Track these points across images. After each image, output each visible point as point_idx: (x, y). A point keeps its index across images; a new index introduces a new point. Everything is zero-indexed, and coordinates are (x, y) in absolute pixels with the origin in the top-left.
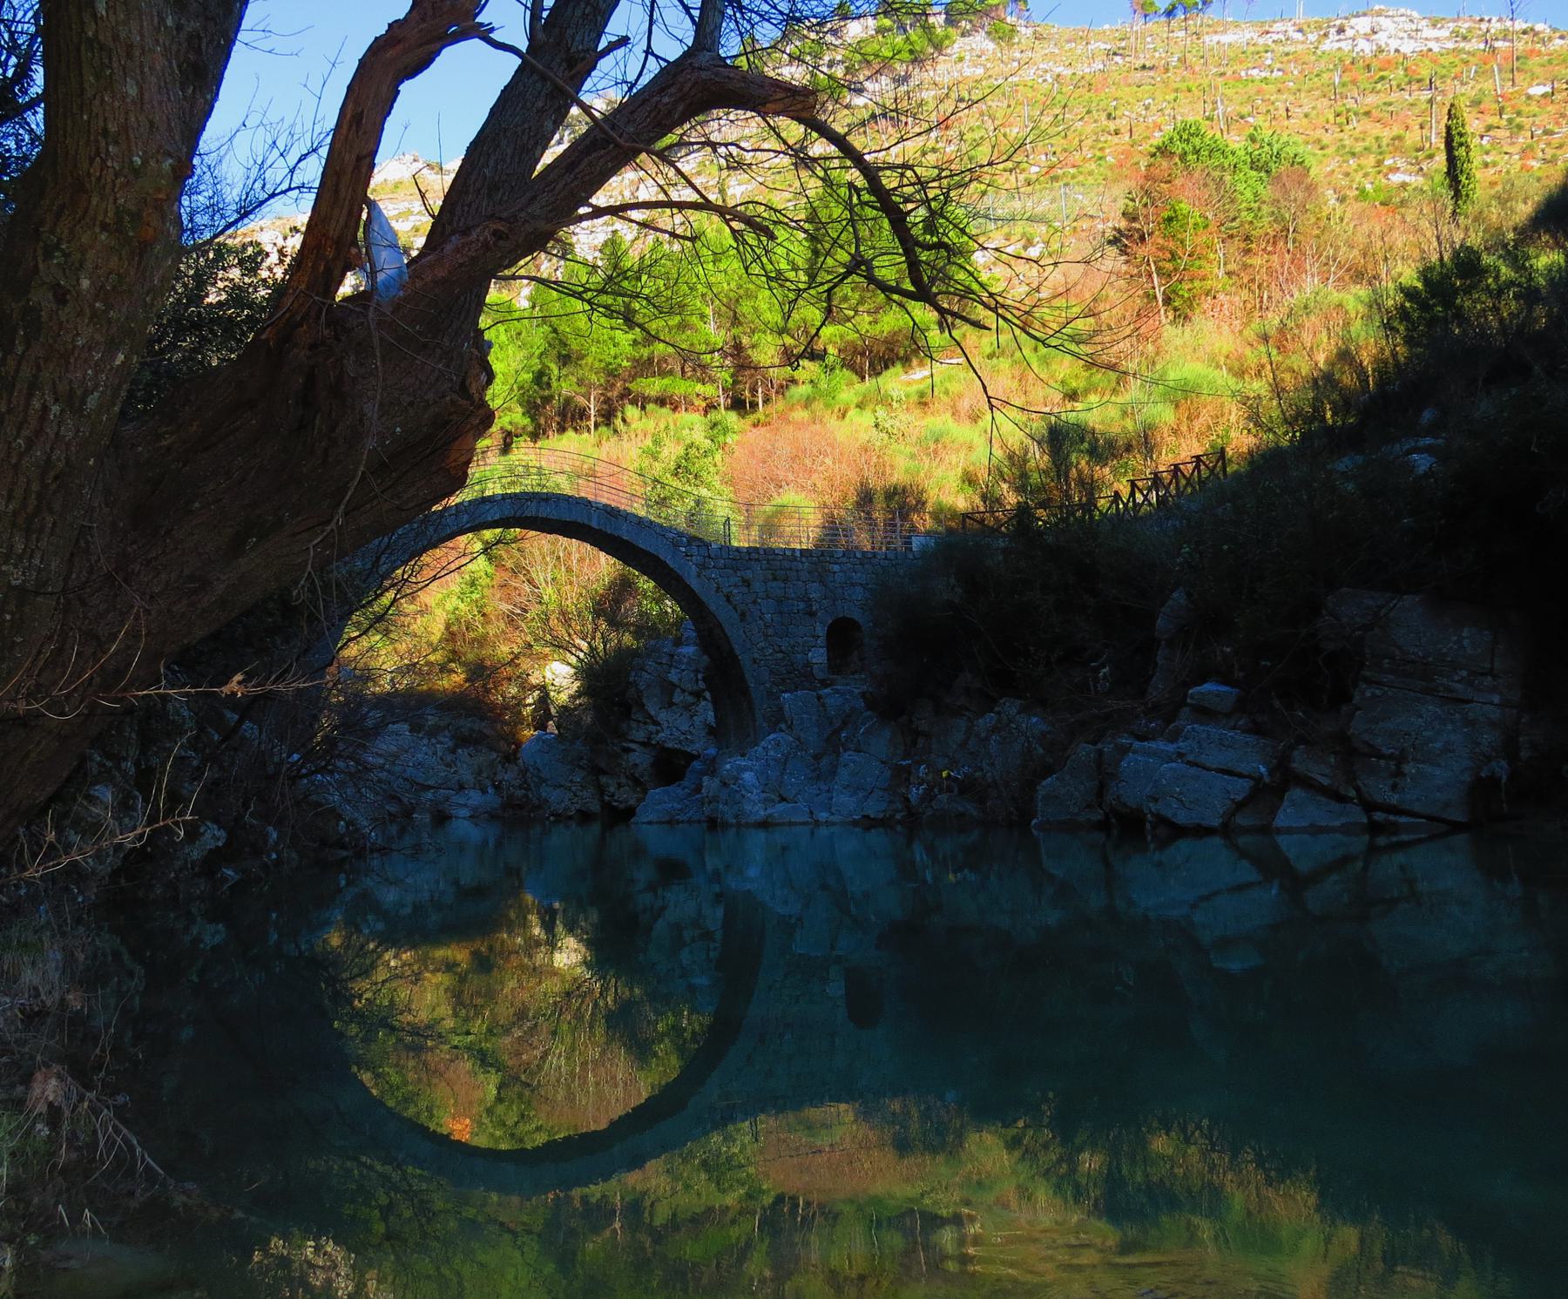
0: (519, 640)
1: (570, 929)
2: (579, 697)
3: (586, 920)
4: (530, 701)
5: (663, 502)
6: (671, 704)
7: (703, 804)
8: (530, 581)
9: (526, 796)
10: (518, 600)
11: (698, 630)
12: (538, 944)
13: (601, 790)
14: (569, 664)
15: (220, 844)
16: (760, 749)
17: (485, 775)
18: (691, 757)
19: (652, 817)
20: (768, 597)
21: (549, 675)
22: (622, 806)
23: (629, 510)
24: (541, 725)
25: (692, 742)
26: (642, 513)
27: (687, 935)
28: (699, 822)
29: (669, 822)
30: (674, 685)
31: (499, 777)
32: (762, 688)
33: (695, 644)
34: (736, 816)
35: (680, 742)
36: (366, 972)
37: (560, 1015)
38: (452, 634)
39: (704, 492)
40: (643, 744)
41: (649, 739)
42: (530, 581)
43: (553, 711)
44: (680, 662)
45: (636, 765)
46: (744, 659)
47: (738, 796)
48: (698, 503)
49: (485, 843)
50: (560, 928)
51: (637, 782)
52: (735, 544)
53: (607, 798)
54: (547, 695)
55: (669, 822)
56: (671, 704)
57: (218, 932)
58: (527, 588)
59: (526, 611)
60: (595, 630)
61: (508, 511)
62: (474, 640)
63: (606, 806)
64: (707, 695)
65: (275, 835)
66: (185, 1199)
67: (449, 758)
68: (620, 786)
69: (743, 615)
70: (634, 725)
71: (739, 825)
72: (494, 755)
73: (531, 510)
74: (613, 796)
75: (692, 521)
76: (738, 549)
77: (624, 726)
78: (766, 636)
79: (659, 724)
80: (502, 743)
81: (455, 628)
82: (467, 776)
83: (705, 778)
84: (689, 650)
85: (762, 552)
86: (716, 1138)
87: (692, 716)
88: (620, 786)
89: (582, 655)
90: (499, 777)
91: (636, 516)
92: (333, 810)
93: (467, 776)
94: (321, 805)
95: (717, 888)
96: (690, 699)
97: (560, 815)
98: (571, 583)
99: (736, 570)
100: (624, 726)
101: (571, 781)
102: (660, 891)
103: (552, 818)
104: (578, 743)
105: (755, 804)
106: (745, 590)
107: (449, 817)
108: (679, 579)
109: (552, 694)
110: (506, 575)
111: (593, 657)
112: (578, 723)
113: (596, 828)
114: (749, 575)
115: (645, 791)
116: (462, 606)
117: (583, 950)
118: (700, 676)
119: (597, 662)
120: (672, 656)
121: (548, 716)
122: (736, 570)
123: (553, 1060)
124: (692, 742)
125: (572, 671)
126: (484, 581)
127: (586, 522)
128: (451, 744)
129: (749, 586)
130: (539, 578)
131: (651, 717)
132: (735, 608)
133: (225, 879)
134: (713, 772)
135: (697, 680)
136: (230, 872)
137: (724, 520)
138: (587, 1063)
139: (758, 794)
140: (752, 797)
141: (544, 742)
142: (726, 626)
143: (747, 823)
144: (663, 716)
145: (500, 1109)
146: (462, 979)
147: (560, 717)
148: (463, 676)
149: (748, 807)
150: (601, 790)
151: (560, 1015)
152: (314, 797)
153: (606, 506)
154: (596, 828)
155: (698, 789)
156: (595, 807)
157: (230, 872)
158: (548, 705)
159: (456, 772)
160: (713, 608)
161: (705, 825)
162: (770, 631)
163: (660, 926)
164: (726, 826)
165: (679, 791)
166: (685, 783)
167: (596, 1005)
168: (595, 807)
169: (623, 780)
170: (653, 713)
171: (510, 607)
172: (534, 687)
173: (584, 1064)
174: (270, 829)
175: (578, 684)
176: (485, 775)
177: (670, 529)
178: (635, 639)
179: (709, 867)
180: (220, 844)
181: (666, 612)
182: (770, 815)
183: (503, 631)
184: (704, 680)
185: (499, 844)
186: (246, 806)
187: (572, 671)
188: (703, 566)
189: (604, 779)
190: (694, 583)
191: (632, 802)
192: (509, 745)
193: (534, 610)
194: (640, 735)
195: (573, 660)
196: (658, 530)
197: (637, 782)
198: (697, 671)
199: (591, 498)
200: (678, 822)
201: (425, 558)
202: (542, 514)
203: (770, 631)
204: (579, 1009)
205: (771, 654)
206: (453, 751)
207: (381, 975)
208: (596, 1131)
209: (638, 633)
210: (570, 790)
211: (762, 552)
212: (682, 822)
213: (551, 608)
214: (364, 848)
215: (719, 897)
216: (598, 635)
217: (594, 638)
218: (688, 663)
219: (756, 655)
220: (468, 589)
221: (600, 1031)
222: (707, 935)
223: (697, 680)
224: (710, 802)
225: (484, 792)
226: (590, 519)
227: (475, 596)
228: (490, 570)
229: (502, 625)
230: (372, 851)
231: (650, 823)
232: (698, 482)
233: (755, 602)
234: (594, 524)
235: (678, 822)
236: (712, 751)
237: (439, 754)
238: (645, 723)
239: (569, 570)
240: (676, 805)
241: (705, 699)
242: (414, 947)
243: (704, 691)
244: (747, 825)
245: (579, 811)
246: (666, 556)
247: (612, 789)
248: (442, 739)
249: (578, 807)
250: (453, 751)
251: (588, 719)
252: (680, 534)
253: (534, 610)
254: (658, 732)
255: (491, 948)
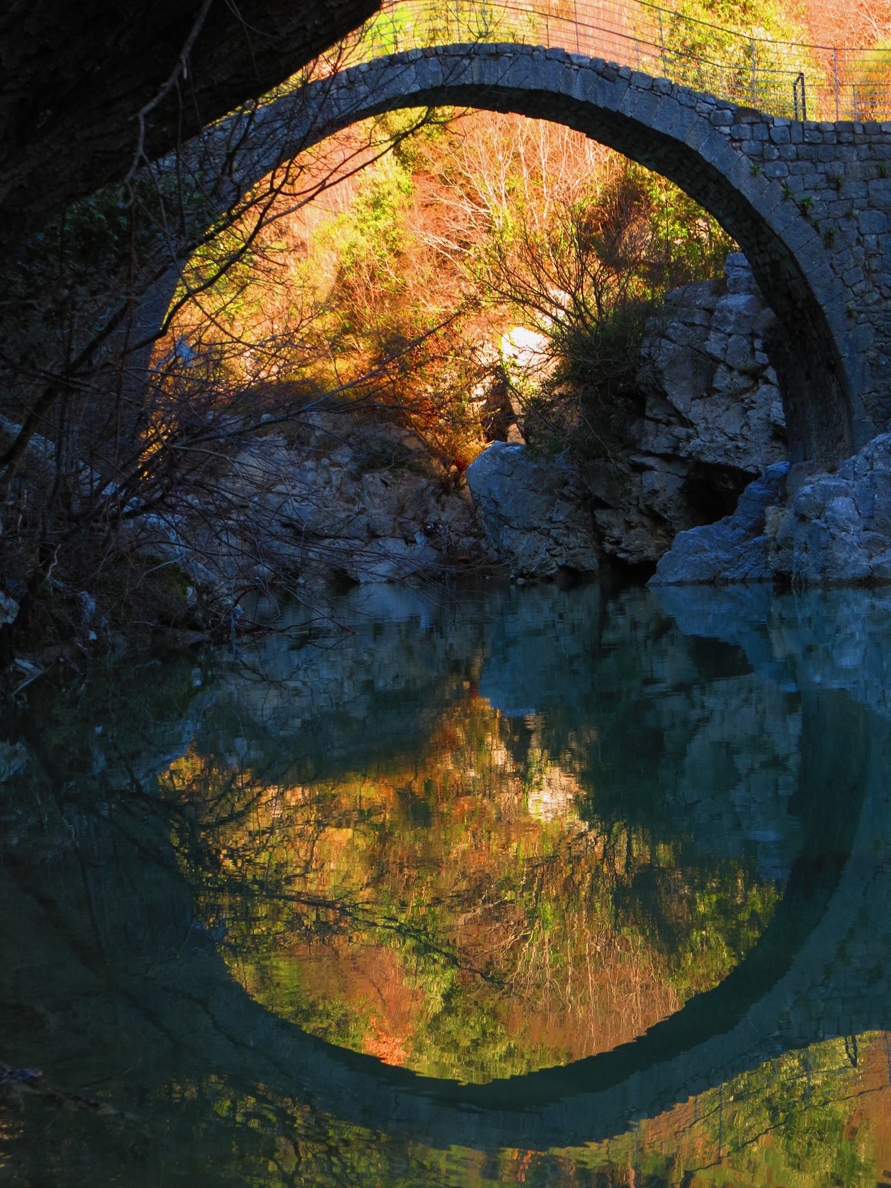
0: (457, 294)
1: (555, 756)
2: (559, 383)
3: (579, 740)
4: (478, 391)
5: (691, 52)
6: (711, 391)
7: (766, 551)
8: (471, 197)
9: (476, 546)
10: (455, 226)
11: (755, 267)
12: (502, 776)
13: (599, 534)
14: (541, 330)
15: (10, 620)
16: (860, 459)
17: (410, 514)
18: (746, 477)
19: (684, 574)
20: (871, 206)
21: (508, 350)
22: (633, 559)
23: (634, 67)
24: (497, 432)
25: (746, 452)
26: (656, 74)
27: (742, 762)
28: (760, 580)
29: (711, 582)
30: (717, 361)
31: (433, 517)
32: (861, 359)
33: (749, 291)
34: (823, 570)
35: (726, 453)
36: (238, 818)
37: (540, 888)
38: (346, 286)
39: (758, 32)
40: (666, 458)
41: (676, 448)
42: (471, 197)
43: (516, 407)
44: (725, 321)
45: (654, 492)
46: (832, 311)
47: (824, 538)
48: (749, 51)
49: (413, 621)
50: (536, 753)
51: (657, 519)
52: (812, 117)
53: (608, 547)
54: (506, 381)
55: (711, 582)
56: (711, 391)
57: (15, 753)
58: (467, 208)
59: (466, 245)
60: (583, 271)
61: (434, 74)
62: (383, 296)
63: (610, 561)
64: (771, 374)
65: (92, 605)
66: (28, 1089)
67: (351, 489)
68: (629, 526)
69: (829, 236)
70: (649, 426)
71: (826, 585)
72: (424, 482)
73: (472, 74)
74: (618, 542)
75: (739, 83)
76: (818, 127)
77: (634, 429)
78: (868, 271)
79: (691, 425)
80: (435, 462)
81: (350, 277)
82: (380, 515)
83: (770, 508)
84: (738, 301)
85: (859, 130)
86: (791, 1063)
87: (745, 411)
88: (629, 526)
89: (561, 315)
90: (433, 517)
91: (643, 76)
92: (175, 569)
93: (380, 515)
94: (158, 562)
95: (791, 688)
96: (742, 382)
97: (533, 575)
98: (539, 197)
99: (815, 161)
100: (634, 429)
101: (550, 520)
102: (696, 692)
103: (520, 581)
104: (560, 457)
105: (853, 548)
106: (831, 195)
107: (355, 583)
108: (721, 180)
109: (514, 380)
110: (431, 187)
111: (580, 316)
112: (558, 427)
113: (591, 593)
114: (837, 169)
115: (670, 534)
116: (362, 241)
117: (575, 787)
118: (758, 344)
119: (587, 326)
120: (710, 311)
121: (509, 416)
122: (815, 161)
123: (531, 952)
124: (746, 452)
125: (546, 341)
126: (396, 199)
127: (563, 90)
128: (352, 467)
129: (838, 187)
130: (485, 188)
131: (677, 413)
132: (816, 227)
133: (21, 675)
134: (782, 500)
135: (753, 350)
136: (27, 665)
137: (794, 78)
138: (582, 958)
139: (857, 533)
140: (848, 539)
141: (503, 458)
142: (801, 258)
143: (840, 580)
144: (697, 411)
145: (450, 1024)
146: (385, 836)
147: (529, 417)
148: (367, 356)
149: (841, 555)
150: (599, 534)
151: (540, 888)
152: (147, 550)
153: (595, 61)
154: (591, 593)
155: (758, 528)
156: (590, 562)
157: (27, 665)
158: (507, 399)
159: (362, 512)
160: (778, 227)
161: (770, 586)
162: (875, 264)
163: (698, 748)
164: (804, 585)
165: (728, 532)
166: (738, 517)
167: (597, 874)
168: (590, 562)
169: (634, 517)
170: (681, 407)
171: (441, 240)
172: (481, 372)
173: (579, 960)
174: (85, 594)
175: (553, 365)
176: (410, 514)
177: (705, 97)
178: (647, 285)
179: (779, 652)
180: (10, 620)
181: (699, 240)
182: (878, 567)
183: (430, 281)
184: (765, 349)
185: (437, 627)
186: (45, 556)
187: (546, 341)
188: (760, 158)
189: (602, 516)
190: (746, 187)
191: (650, 552)
192: (446, 464)
193: (482, 242)
194: (660, 443)
195: (547, 323)
196: (684, 99)
197: (657, 519)
198: (753, 335)
199: (569, 49)
200: (726, 582)
201: (305, 157)
202: (489, 80)
203: (875, 264)
204: (570, 878)
205: (878, 302)
206: (356, 477)
207: (258, 820)
208: (601, 1056)
209: (653, 275)
210: (548, 534)
211: (859, 130)
212: (733, 581)
213: (509, 238)
214: (227, 628)
215: (793, 701)
216: (588, 280)
217: (579, 286)
218: (738, 323)
219: (852, 305)
220: (368, 213)
221: (603, 912)
222: (777, 763)
223: (753, 350)
224: (779, 549)
225: (409, 541)
226: (569, 84)
227: (382, 224)
228: (405, 179)
229: (428, 270)
230: (239, 633)
231: (680, 584)
232: (748, 17)
233: (848, 216)
234: (577, 93)
235: (726, 582)
236: (779, 466)
237: (336, 481)
238: (668, 424)
239: (534, 175)
240: (721, 554)
241: (767, 382)
242: (304, 781)
243: (764, 367)
244: (841, 584)
245: (562, 568)
246: (695, 141)
247: (616, 532)
248: (339, 459)
249: (561, 561)
250: (356, 477)
251: (573, 419)
252: (722, 105)
253: (482, 242)
254: (689, 438)
255: (428, 786)
